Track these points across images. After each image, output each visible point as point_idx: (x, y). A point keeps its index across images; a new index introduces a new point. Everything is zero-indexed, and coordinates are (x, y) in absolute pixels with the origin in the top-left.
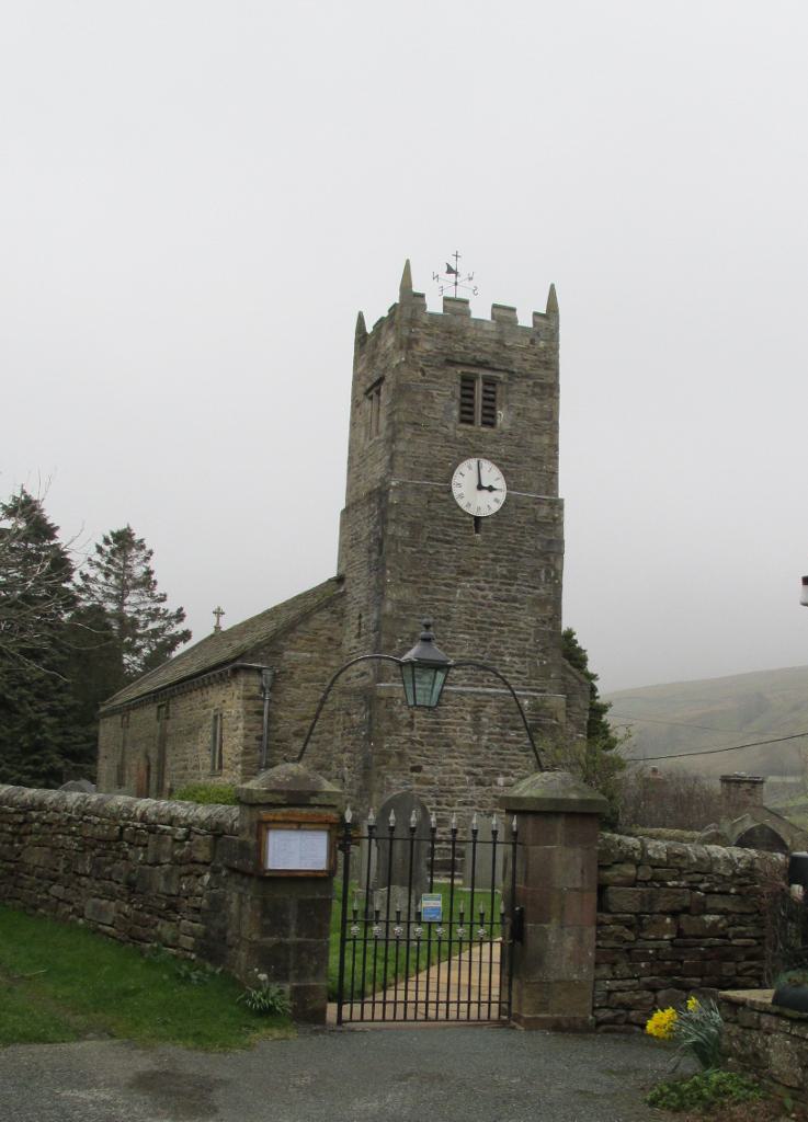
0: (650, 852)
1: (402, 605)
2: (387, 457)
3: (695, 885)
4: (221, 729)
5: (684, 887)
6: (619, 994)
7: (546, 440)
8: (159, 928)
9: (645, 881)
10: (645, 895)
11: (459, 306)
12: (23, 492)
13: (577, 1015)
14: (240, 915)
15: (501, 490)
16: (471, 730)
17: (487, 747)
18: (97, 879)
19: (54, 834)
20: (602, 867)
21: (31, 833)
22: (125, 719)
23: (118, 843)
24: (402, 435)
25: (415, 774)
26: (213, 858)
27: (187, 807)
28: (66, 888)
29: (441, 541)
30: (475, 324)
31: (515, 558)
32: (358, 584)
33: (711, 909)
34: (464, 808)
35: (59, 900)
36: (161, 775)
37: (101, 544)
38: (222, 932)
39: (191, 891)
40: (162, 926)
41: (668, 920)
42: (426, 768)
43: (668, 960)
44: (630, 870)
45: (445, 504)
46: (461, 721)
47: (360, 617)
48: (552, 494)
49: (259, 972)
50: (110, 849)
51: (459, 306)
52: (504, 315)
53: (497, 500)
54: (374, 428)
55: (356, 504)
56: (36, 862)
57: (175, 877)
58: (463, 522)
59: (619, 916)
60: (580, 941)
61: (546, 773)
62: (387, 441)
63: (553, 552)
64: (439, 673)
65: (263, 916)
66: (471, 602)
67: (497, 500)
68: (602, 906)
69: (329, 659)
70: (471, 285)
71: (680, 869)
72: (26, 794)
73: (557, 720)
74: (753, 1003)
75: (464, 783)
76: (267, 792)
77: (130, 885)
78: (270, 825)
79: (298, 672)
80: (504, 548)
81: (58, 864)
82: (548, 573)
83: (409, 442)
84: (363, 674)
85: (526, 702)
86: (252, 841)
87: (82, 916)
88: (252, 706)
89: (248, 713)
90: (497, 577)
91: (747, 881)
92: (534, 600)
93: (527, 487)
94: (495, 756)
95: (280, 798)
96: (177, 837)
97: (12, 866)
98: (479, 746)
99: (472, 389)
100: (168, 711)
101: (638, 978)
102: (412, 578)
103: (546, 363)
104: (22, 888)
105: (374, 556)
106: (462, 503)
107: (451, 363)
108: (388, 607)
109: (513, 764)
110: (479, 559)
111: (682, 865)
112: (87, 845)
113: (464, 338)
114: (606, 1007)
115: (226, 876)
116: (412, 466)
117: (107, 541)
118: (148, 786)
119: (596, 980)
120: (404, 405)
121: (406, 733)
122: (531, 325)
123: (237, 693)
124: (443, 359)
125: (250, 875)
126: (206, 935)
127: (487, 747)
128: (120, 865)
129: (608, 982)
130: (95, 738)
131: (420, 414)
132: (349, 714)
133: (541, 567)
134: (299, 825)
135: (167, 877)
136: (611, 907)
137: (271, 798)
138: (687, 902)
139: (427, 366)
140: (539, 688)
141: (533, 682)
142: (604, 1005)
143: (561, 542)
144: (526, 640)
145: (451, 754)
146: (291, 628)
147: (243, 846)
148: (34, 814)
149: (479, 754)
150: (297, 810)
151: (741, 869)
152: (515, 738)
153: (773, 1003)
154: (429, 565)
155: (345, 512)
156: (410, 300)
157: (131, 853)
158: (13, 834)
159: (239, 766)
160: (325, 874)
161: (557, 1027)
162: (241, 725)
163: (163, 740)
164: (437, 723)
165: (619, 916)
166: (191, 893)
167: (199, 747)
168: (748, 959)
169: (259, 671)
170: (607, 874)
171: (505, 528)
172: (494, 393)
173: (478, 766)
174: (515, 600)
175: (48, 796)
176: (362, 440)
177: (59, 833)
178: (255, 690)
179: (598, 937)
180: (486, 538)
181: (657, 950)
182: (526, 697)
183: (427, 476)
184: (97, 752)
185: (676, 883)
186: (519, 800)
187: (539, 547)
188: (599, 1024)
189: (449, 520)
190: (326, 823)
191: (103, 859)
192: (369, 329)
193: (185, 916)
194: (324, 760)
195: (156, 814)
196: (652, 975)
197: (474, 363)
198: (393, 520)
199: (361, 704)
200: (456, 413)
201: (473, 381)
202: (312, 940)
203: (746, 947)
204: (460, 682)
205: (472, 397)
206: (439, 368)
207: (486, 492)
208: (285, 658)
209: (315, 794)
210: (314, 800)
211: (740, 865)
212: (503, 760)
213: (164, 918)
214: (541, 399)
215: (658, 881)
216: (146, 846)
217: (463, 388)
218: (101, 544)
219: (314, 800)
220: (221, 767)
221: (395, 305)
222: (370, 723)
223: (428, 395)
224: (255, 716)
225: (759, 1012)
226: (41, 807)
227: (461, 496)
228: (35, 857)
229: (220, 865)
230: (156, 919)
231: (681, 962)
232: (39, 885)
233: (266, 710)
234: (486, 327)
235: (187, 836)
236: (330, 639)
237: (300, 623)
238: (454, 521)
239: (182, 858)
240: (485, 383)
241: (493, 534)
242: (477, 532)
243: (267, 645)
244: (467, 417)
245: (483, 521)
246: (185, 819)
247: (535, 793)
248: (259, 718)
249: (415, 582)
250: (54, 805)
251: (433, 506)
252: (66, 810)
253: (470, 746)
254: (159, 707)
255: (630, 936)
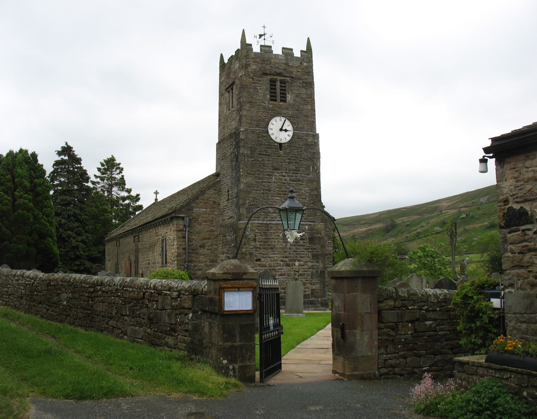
0: (400, 294)
1: (248, 185)
2: (238, 118)
3: (421, 308)
4: (166, 245)
5: (416, 309)
6: (389, 361)
7: (309, 107)
8: (167, 339)
9: (399, 307)
10: (399, 314)
11: (268, 49)
12: (66, 143)
13: (371, 372)
14: (211, 333)
15: (291, 131)
16: (282, 241)
17: (290, 249)
18: (133, 317)
19: (109, 297)
20: (379, 302)
21: (97, 296)
22: (118, 242)
23: (143, 300)
24: (244, 107)
25: (258, 263)
26: (193, 306)
27: (177, 282)
28: (117, 322)
29: (265, 155)
30: (275, 56)
31: (299, 161)
32: (226, 176)
33: (430, 318)
34: (281, 277)
35: (114, 327)
36: (137, 268)
37: (100, 166)
38: (201, 341)
39: (183, 322)
40: (168, 339)
41: (410, 325)
42: (262, 259)
43: (411, 343)
44: (391, 303)
45: (265, 138)
46: (277, 237)
47: (228, 191)
48: (314, 132)
49: (223, 360)
50: (139, 303)
51: (268, 49)
52: (287, 52)
53: (289, 135)
54: (231, 105)
55: (224, 140)
56: (101, 310)
57: (173, 316)
58: (274, 146)
59: (388, 324)
60: (371, 337)
61: (350, 259)
62: (238, 110)
63: (316, 158)
64: (297, 214)
65: (224, 333)
66: (280, 182)
67: (289, 135)
68: (380, 320)
69: (215, 211)
70: (272, 39)
71: (414, 301)
72: (94, 279)
73: (321, 235)
74: (473, 363)
75: (280, 266)
76: (223, 273)
77: (150, 319)
78: (225, 290)
79: (200, 218)
80: (293, 157)
81: (112, 311)
82: (313, 167)
83: (248, 110)
84: (231, 218)
85: (307, 227)
86: (217, 298)
87: (126, 335)
88: (180, 234)
89: (179, 237)
90: (290, 171)
91: (444, 304)
92: (308, 180)
93: (302, 129)
94: (294, 253)
95: (229, 277)
96: (173, 297)
97: (89, 312)
98: (286, 248)
99: (275, 86)
100: (139, 238)
101: (398, 353)
102: (252, 172)
103: (307, 72)
104: (95, 322)
105: (234, 163)
106: (273, 137)
107: (265, 74)
108: (242, 186)
109: (301, 256)
110: (282, 162)
111: (414, 299)
112: (126, 301)
113: (270, 63)
114: (384, 367)
115: (201, 314)
116: (250, 121)
117: (102, 165)
118: (131, 272)
119: (378, 355)
120: (245, 94)
121: (253, 243)
122: (300, 56)
123: (173, 228)
124: (261, 72)
125: (216, 314)
126: (192, 342)
127: (290, 249)
128: (145, 310)
129: (384, 356)
130: (103, 252)
131: (252, 97)
132: (225, 236)
133: (310, 165)
134: (239, 289)
135: (169, 316)
136: (384, 320)
137: (225, 277)
138: (417, 316)
139: (254, 76)
140: (312, 220)
141: (309, 218)
142: (383, 366)
143: (319, 153)
144: (305, 199)
145: (274, 253)
146: (196, 198)
147: (211, 300)
148: (99, 288)
149: (286, 252)
150: (237, 282)
151: (441, 299)
152: (302, 244)
153: (485, 362)
154: (260, 167)
155: (219, 144)
156: (245, 47)
157: (150, 305)
158: (89, 297)
159: (176, 262)
160: (252, 312)
161: (362, 378)
162: (175, 243)
163: (137, 251)
164: (267, 239)
165: (388, 324)
166: (182, 323)
167: (155, 254)
168: (446, 340)
169: (183, 218)
170: (382, 305)
171: (293, 148)
172: (285, 87)
173: (286, 257)
174: (299, 180)
175: (105, 279)
176: (225, 111)
177: (112, 296)
178: (182, 227)
179: (379, 335)
180: (285, 153)
181: (405, 339)
182: (306, 225)
183: (257, 126)
184: (105, 258)
185: (412, 307)
186: (339, 272)
187: (309, 156)
188: (381, 375)
189: (267, 145)
190: (252, 287)
191: (135, 308)
192: (226, 61)
193: (180, 333)
194: (214, 258)
195: (161, 286)
196: (404, 351)
197: (275, 74)
198: (242, 146)
199: (231, 231)
200: (268, 96)
201: (275, 82)
202: (247, 343)
203: (444, 335)
204: (277, 219)
205: (275, 89)
206: (259, 77)
207: (284, 132)
208: (194, 211)
209: (245, 273)
210: (245, 277)
211: (440, 297)
212: (298, 254)
213: (169, 335)
214: (306, 89)
215: (404, 307)
216: (157, 301)
217: (271, 85)
218: (100, 166)
219: (245, 277)
220: (166, 263)
221: (238, 50)
222: (236, 240)
223: (255, 88)
224: (182, 239)
225: (477, 367)
226: (102, 284)
227: (273, 134)
228: (100, 308)
229: (197, 309)
230: (165, 335)
231: (416, 344)
232: (104, 320)
233: (187, 235)
234: (280, 58)
235: (179, 296)
236: (214, 202)
237: (200, 195)
238: (270, 145)
239: (176, 306)
240: (281, 83)
241: (288, 151)
242: (280, 150)
243: (186, 206)
244: (273, 98)
245: (283, 145)
246: (177, 288)
247: (348, 268)
248: (184, 239)
249: (253, 174)
250: (108, 283)
251: (260, 139)
252: (114, 285)
253: (282, 248)
254: (134, 237)
255: (393, 333)
